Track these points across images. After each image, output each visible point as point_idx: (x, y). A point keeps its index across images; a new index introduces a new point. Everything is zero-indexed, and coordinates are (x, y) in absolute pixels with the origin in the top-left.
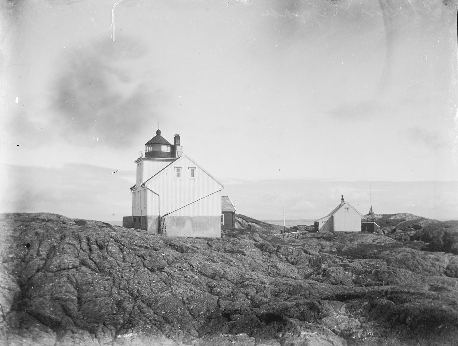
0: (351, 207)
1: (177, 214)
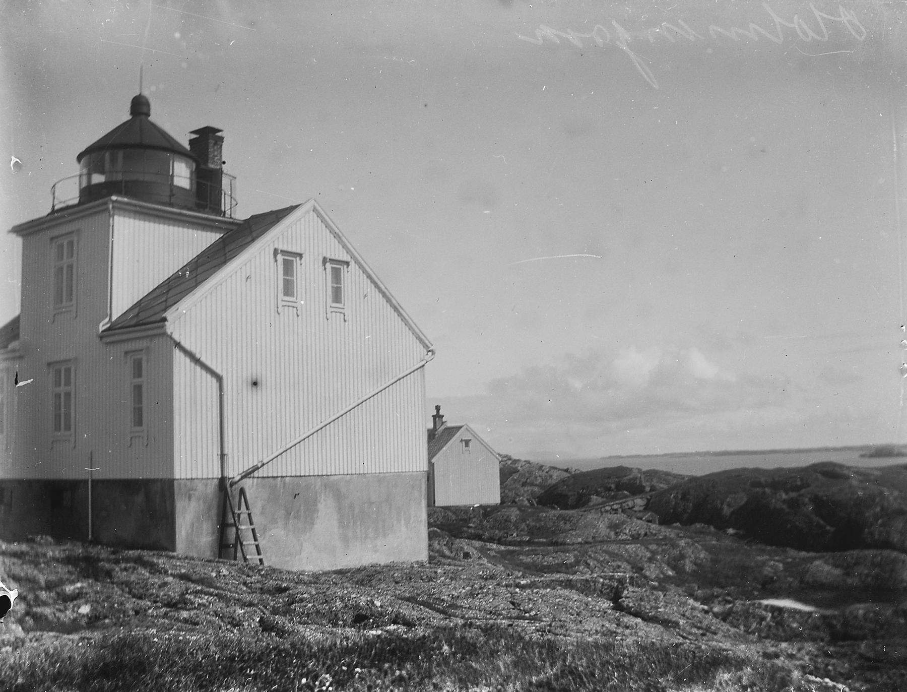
0: (475, 436)
1: (287, 467)
